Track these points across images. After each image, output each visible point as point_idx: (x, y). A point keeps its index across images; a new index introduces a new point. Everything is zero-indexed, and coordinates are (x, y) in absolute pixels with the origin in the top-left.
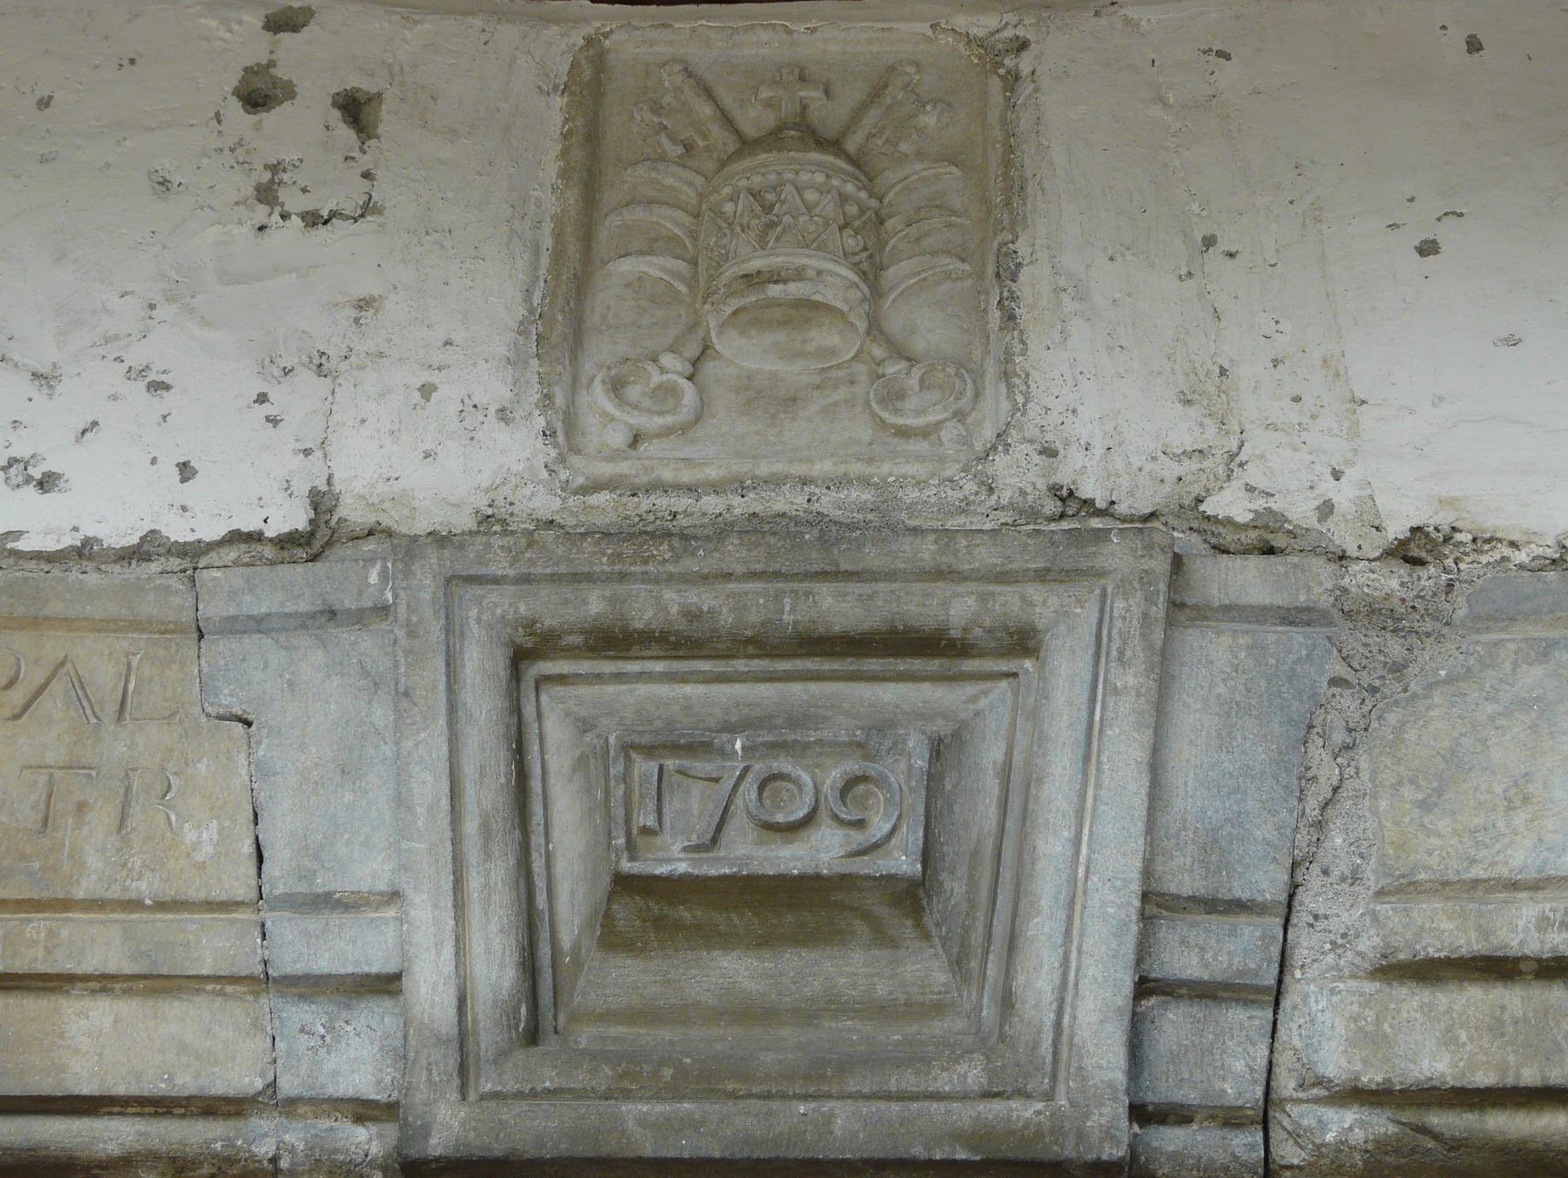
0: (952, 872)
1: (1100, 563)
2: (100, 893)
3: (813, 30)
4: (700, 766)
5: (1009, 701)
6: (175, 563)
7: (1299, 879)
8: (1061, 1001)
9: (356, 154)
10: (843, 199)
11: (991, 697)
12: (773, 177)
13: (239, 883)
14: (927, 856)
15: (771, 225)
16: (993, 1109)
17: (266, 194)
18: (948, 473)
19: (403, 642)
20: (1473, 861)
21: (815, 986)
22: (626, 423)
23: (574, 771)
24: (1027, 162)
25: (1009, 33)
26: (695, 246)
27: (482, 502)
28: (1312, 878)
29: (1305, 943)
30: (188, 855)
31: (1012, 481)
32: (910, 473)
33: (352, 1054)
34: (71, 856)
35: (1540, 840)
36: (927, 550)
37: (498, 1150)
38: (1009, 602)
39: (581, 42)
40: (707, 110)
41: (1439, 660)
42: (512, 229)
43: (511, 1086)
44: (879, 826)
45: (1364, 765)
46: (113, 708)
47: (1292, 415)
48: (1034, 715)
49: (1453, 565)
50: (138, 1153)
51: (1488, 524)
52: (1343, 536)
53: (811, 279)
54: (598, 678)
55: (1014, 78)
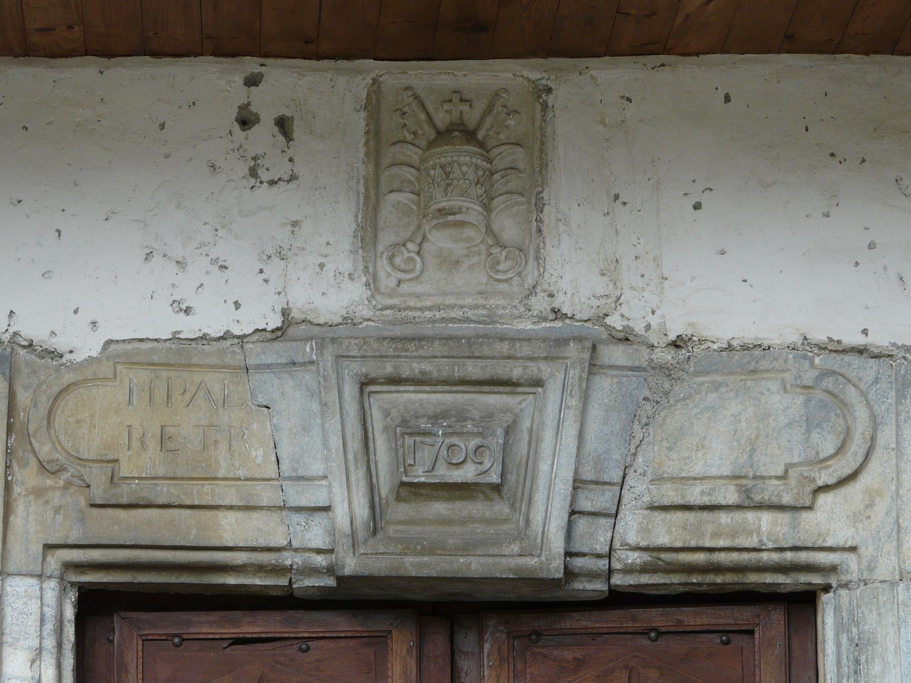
0: (511, 473)
1: (566, 354)
2: (227, 475)
3: (465, 75)
4: (427, 440)
5: (533, 403)
6: (236, 341)
7: (627, 473)
8: (545, 523)
9: (286, 149)
10: (477, 168)
11: (527, 402)
12: (449, 159)
13: (272, 471)
14: (503, 475)
15: (449, 185)
16: (522, 561)
17: (253, 173)
18: (514, 304)
19: (322, 383)
20: (683, 470)
21: (465, 513)
22: (396, 277)
23: (384, 431)
24: (549, 152)
25: (544, 82)
26: (419, 187)
27: (344, 313)
28: (630, 472)
29: (627, 497)
30: (254, 461)
31: (538, 307)
32: (500, 304)
33: (315, 532)
34: (215, 461)
35: (706, 462)
37: (367, 573)
38: (533, 369)
39: (371, 82)
40: (423, 116)
41: (680, 390)
42: (349, 186)
43: (369, 551)
44: (487, 465)
45: (651, 432)
46: (221, 402)
47: (640, 283)
48: (541, 411)
49: (691, 349)
50: (248, 564)
51: (704, 335)
52: (653, 339)
53: (464, 213)
54: (391, 392)
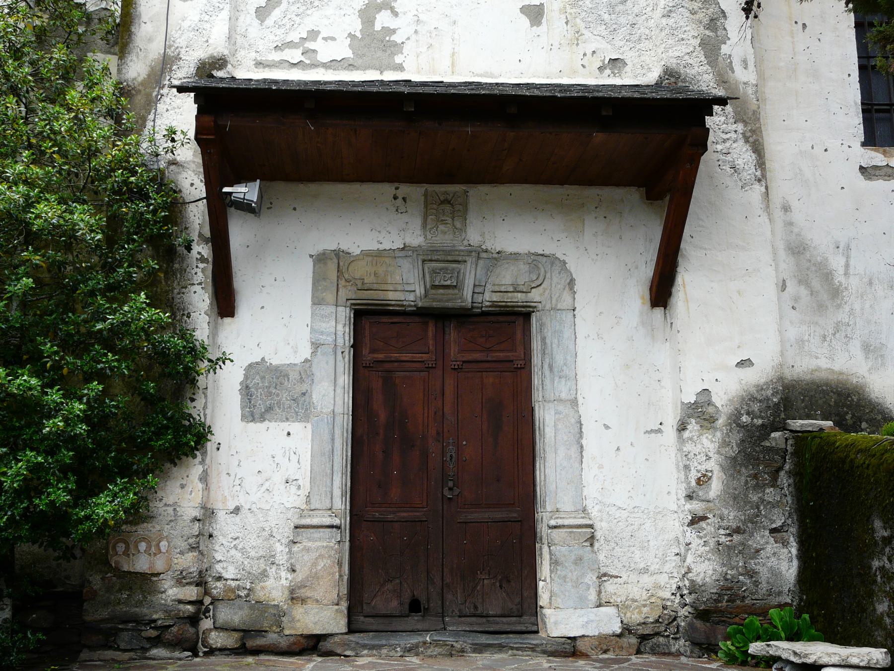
13: (401, 282)
36: (457, 253)
55: (467, 196)
